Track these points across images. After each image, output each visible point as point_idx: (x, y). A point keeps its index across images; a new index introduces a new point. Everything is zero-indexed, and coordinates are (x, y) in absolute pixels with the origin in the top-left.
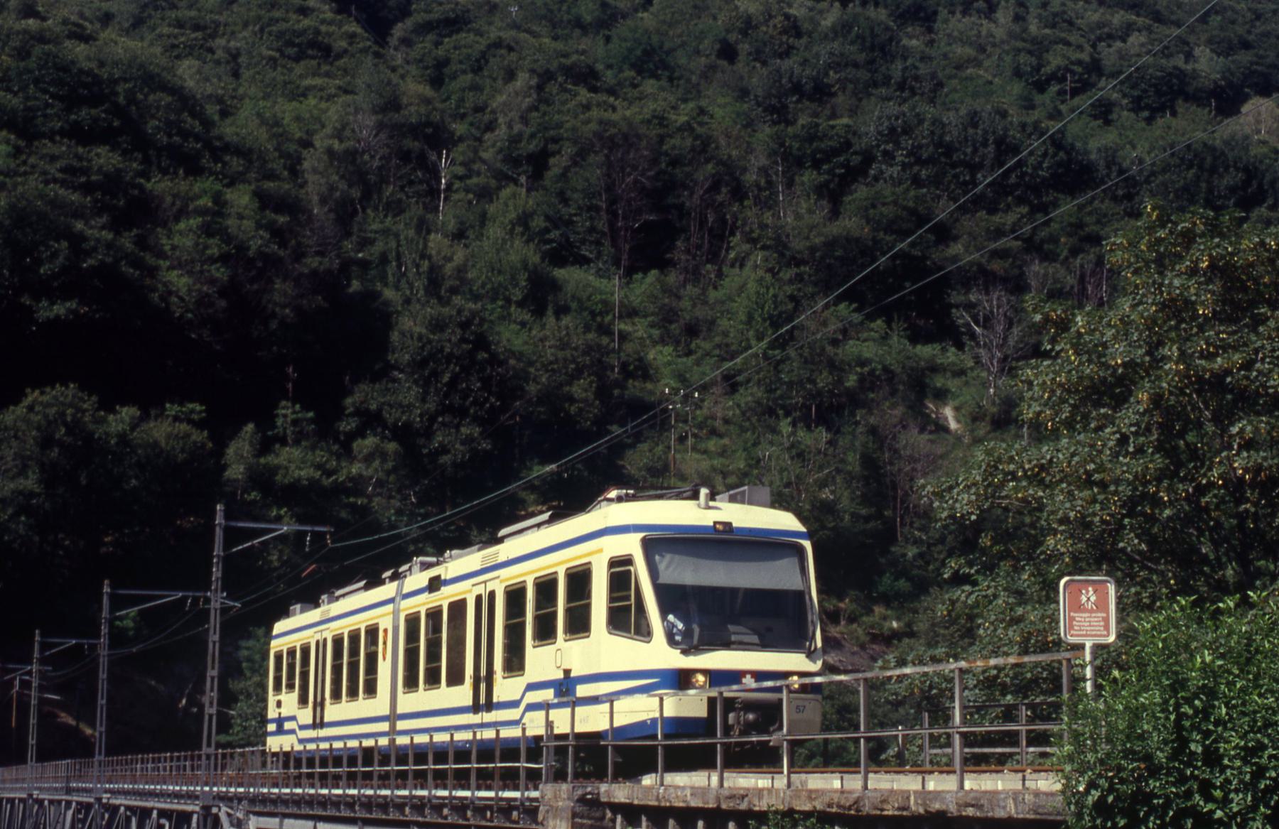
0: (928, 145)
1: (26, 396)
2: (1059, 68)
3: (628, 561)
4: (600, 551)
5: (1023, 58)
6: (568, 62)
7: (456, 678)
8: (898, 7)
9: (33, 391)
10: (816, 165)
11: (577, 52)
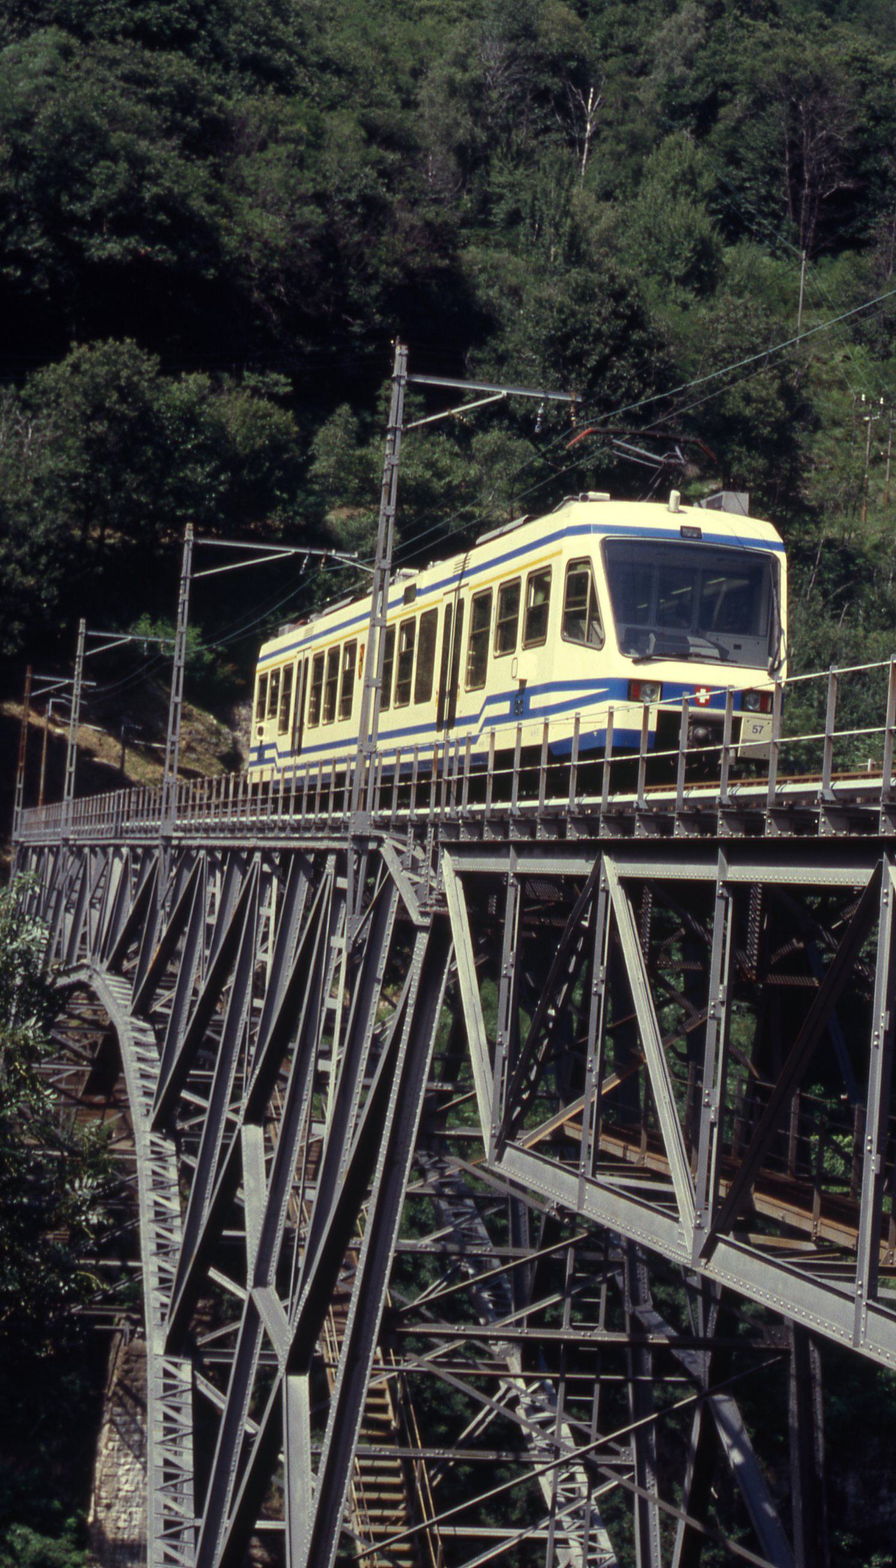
1: (71, 351)
3: (586, 561)
4: (560, 553)
7: (423, 696)
9: (80, 346)
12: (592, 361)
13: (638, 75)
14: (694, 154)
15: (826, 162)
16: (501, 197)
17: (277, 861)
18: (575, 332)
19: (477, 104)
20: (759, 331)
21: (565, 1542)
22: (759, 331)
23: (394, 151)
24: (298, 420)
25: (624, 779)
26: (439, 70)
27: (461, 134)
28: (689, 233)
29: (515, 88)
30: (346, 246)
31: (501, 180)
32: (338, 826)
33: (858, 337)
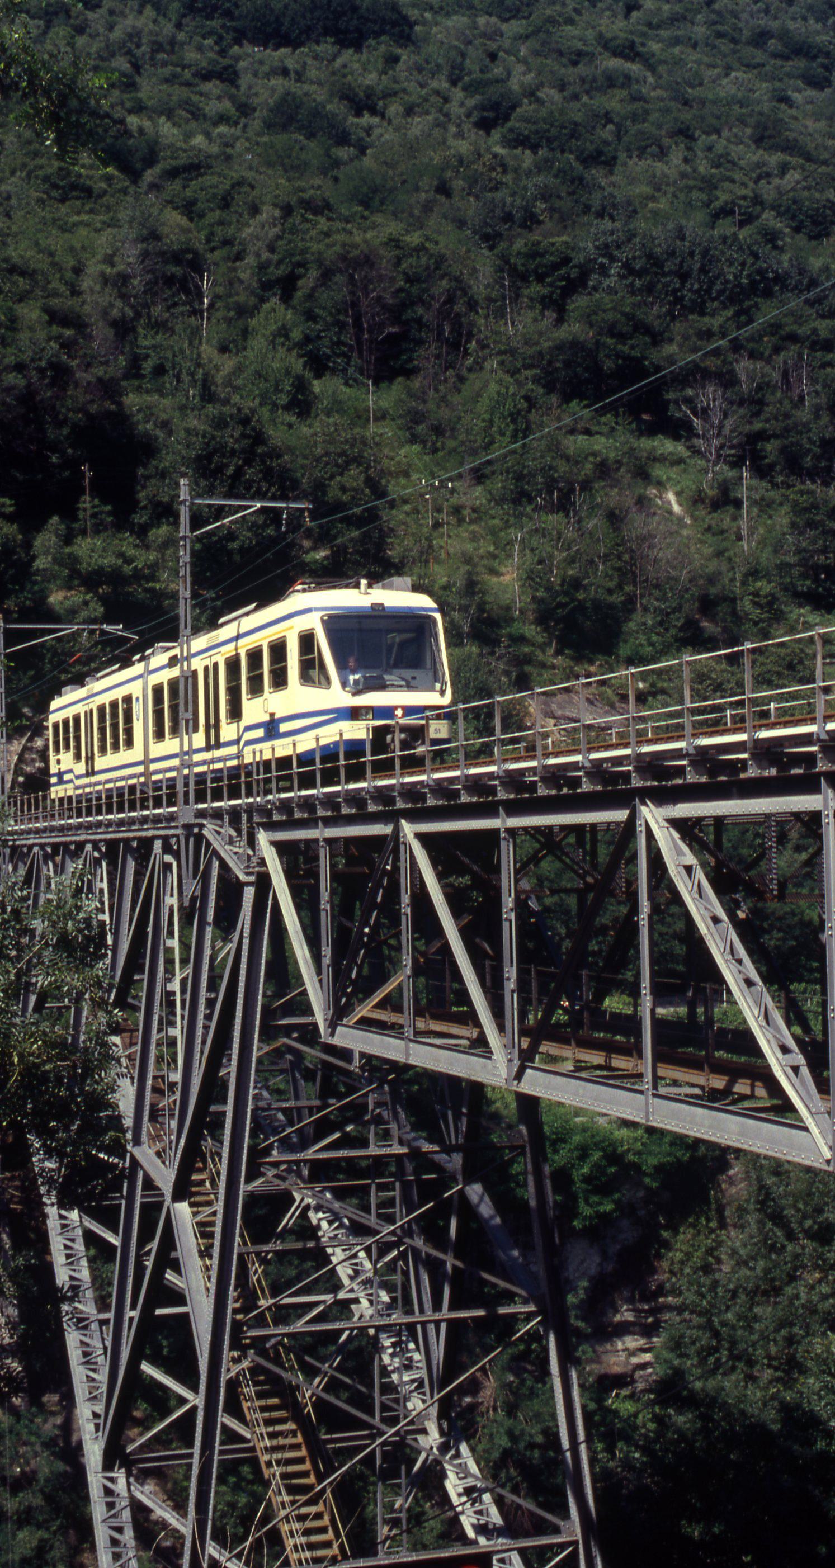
0: (640, 258)
2: (726, 203)
5: (695, 194)
6: (306, 196)
8: (582, 152)
10: (540, 279)
11: (313, 187)
12: (230, 471)
13: (234, 261)
14: (285, 315)
15: (378, 314)
16: (148, 356)
17: (103, 849)
18: (215, 451)
19: (124, 290)
20: (347, 441)
21: (357, 1301)
22: (347, 441)
23: (69, 328)
24: (22, 530)
25: (356, 773)
26: (94, 268)
27: (115, 313)
28: (288, 373)
29: (149, 276)
30: (42, 401)
31: (146, 343)
32: (172, 817)
33: (413, 439)
